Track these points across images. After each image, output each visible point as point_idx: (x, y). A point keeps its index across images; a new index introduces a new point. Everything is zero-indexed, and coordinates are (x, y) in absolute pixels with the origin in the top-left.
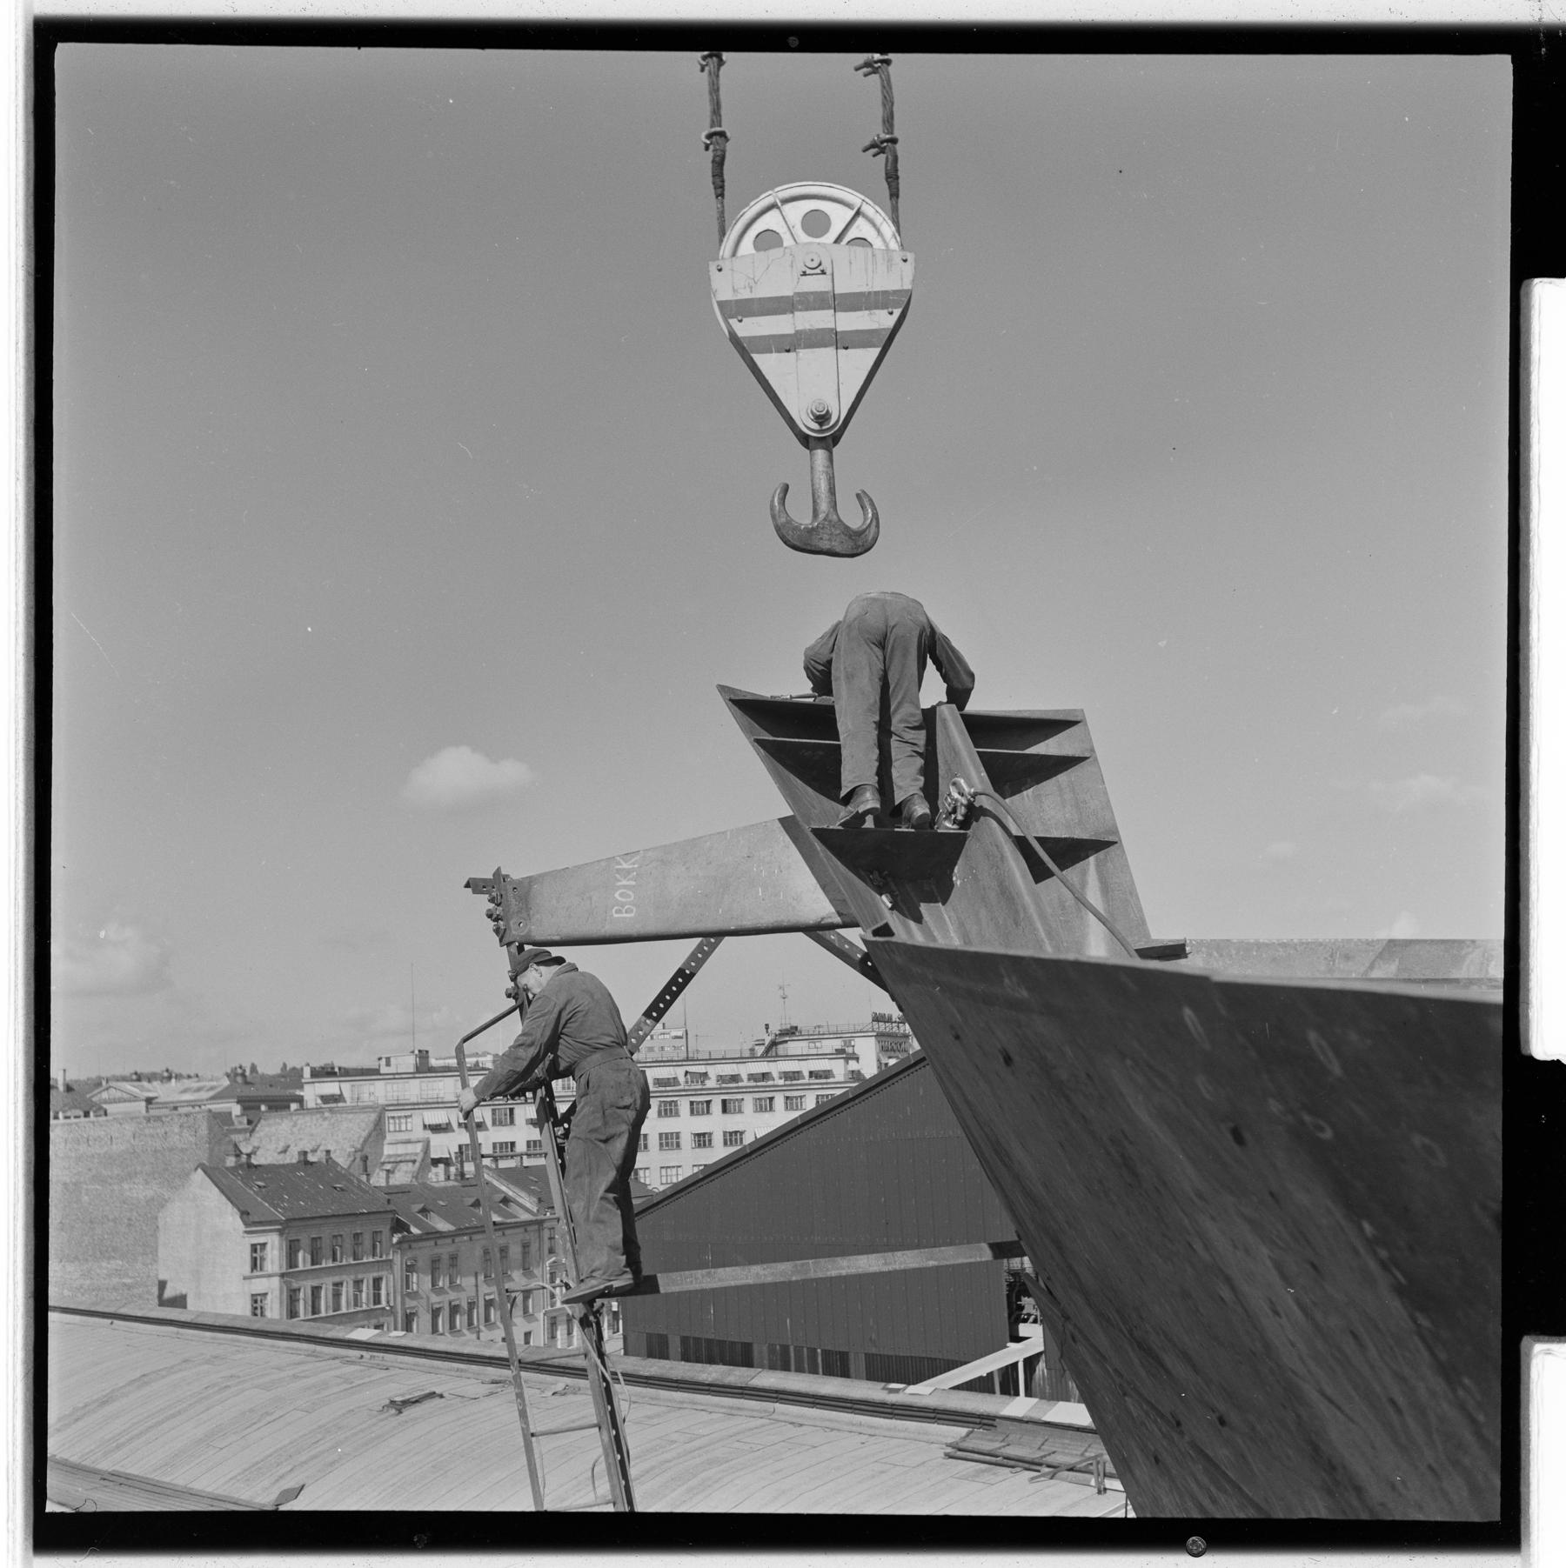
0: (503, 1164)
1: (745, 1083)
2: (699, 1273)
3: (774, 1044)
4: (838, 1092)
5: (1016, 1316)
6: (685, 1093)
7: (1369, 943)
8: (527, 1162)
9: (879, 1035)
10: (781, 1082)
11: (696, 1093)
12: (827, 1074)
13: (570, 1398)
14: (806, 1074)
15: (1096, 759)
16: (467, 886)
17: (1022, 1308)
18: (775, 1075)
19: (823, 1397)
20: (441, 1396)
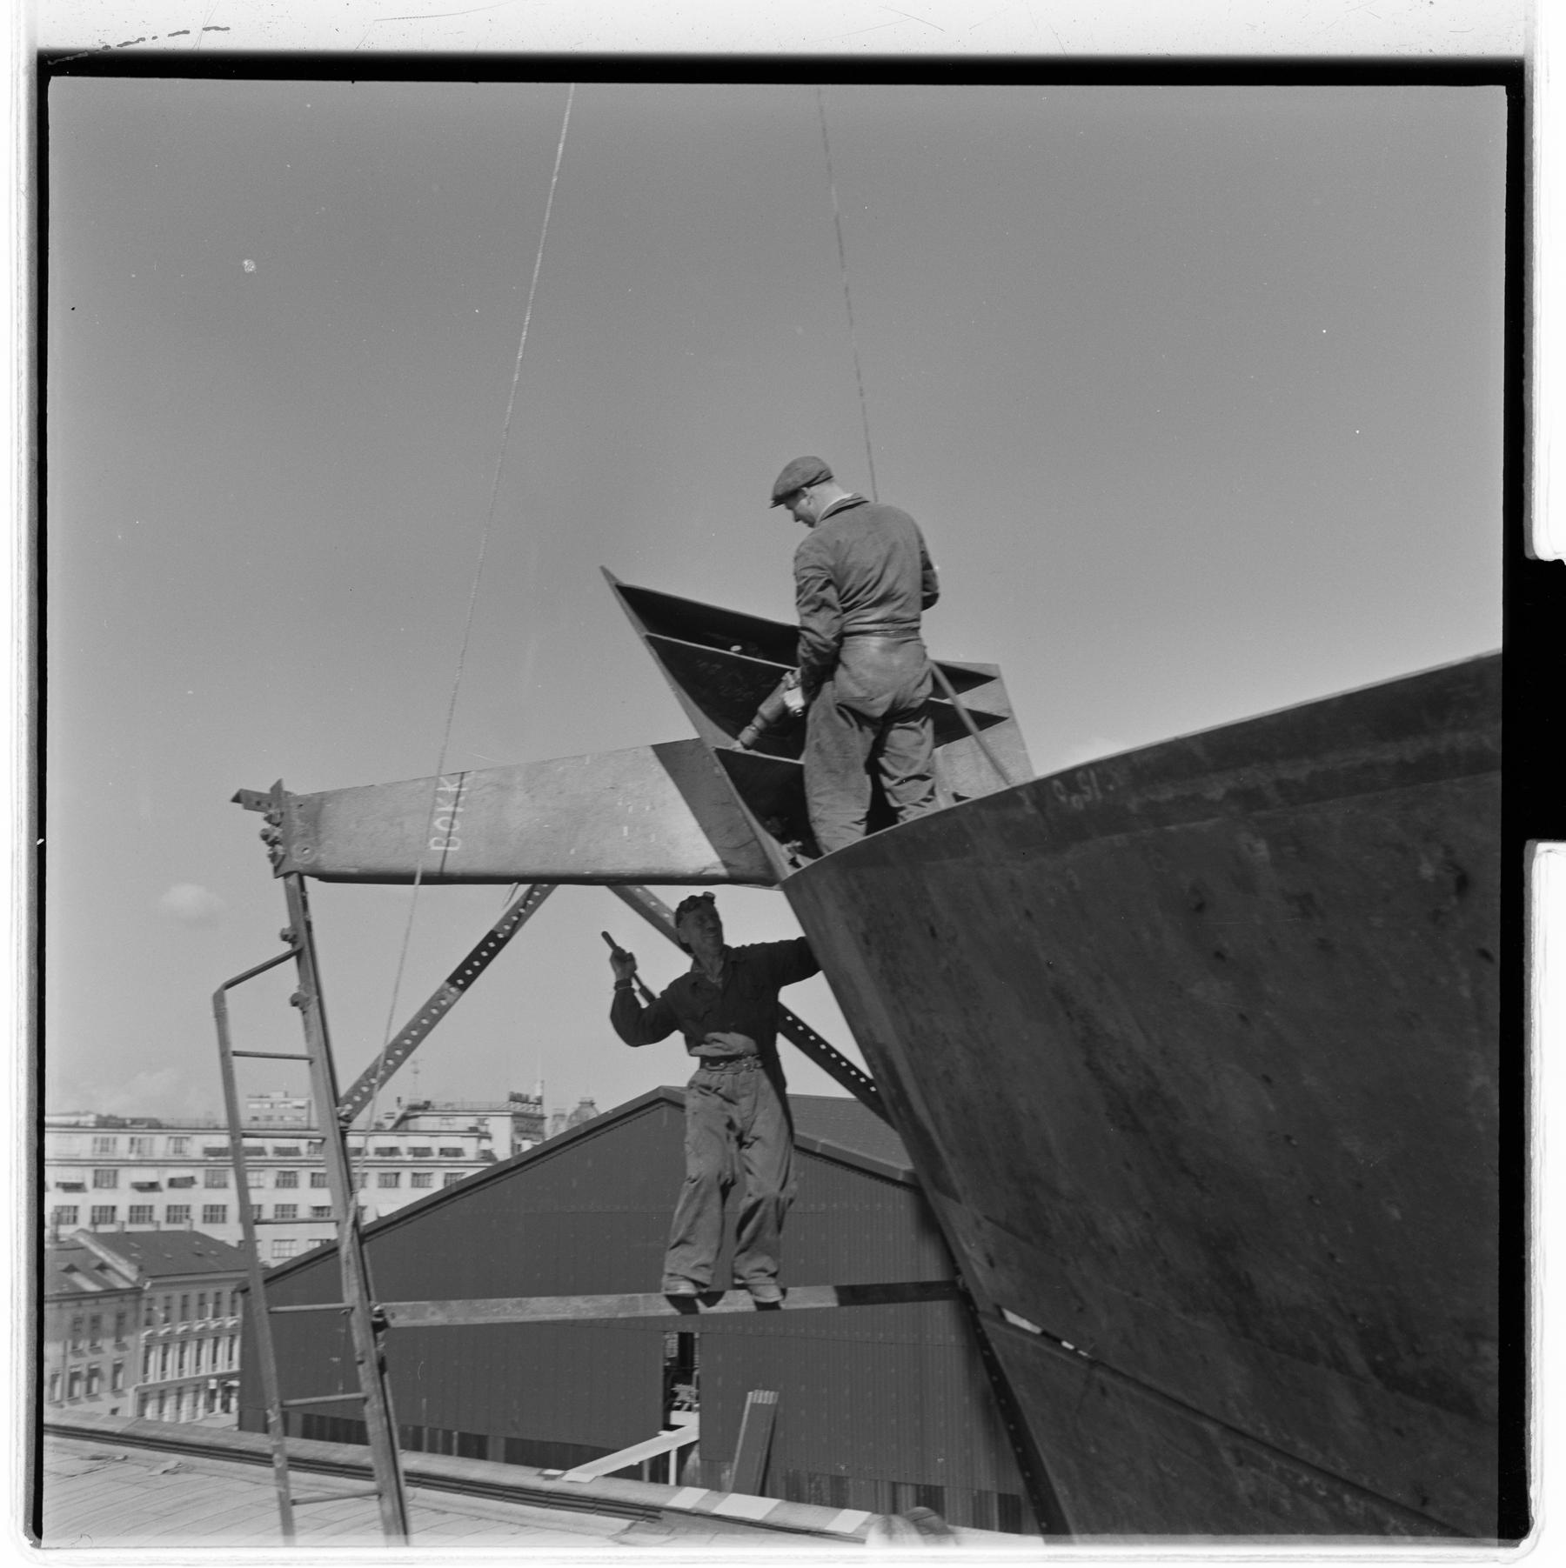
0: (102, 1229)
1: (372, 1157)
3: (405, 1118)
4: (470, 1172)
5: (670, 1402)
8: (129, 1228)
10: (410, 1158)
12: (457, 1152)
13: (182, 1477)
14: (436, 1151)
15: (1014, 722)
16: (237, 799)
17: (675, 1395)
18: (403, 1150)
19: (471, 1483)
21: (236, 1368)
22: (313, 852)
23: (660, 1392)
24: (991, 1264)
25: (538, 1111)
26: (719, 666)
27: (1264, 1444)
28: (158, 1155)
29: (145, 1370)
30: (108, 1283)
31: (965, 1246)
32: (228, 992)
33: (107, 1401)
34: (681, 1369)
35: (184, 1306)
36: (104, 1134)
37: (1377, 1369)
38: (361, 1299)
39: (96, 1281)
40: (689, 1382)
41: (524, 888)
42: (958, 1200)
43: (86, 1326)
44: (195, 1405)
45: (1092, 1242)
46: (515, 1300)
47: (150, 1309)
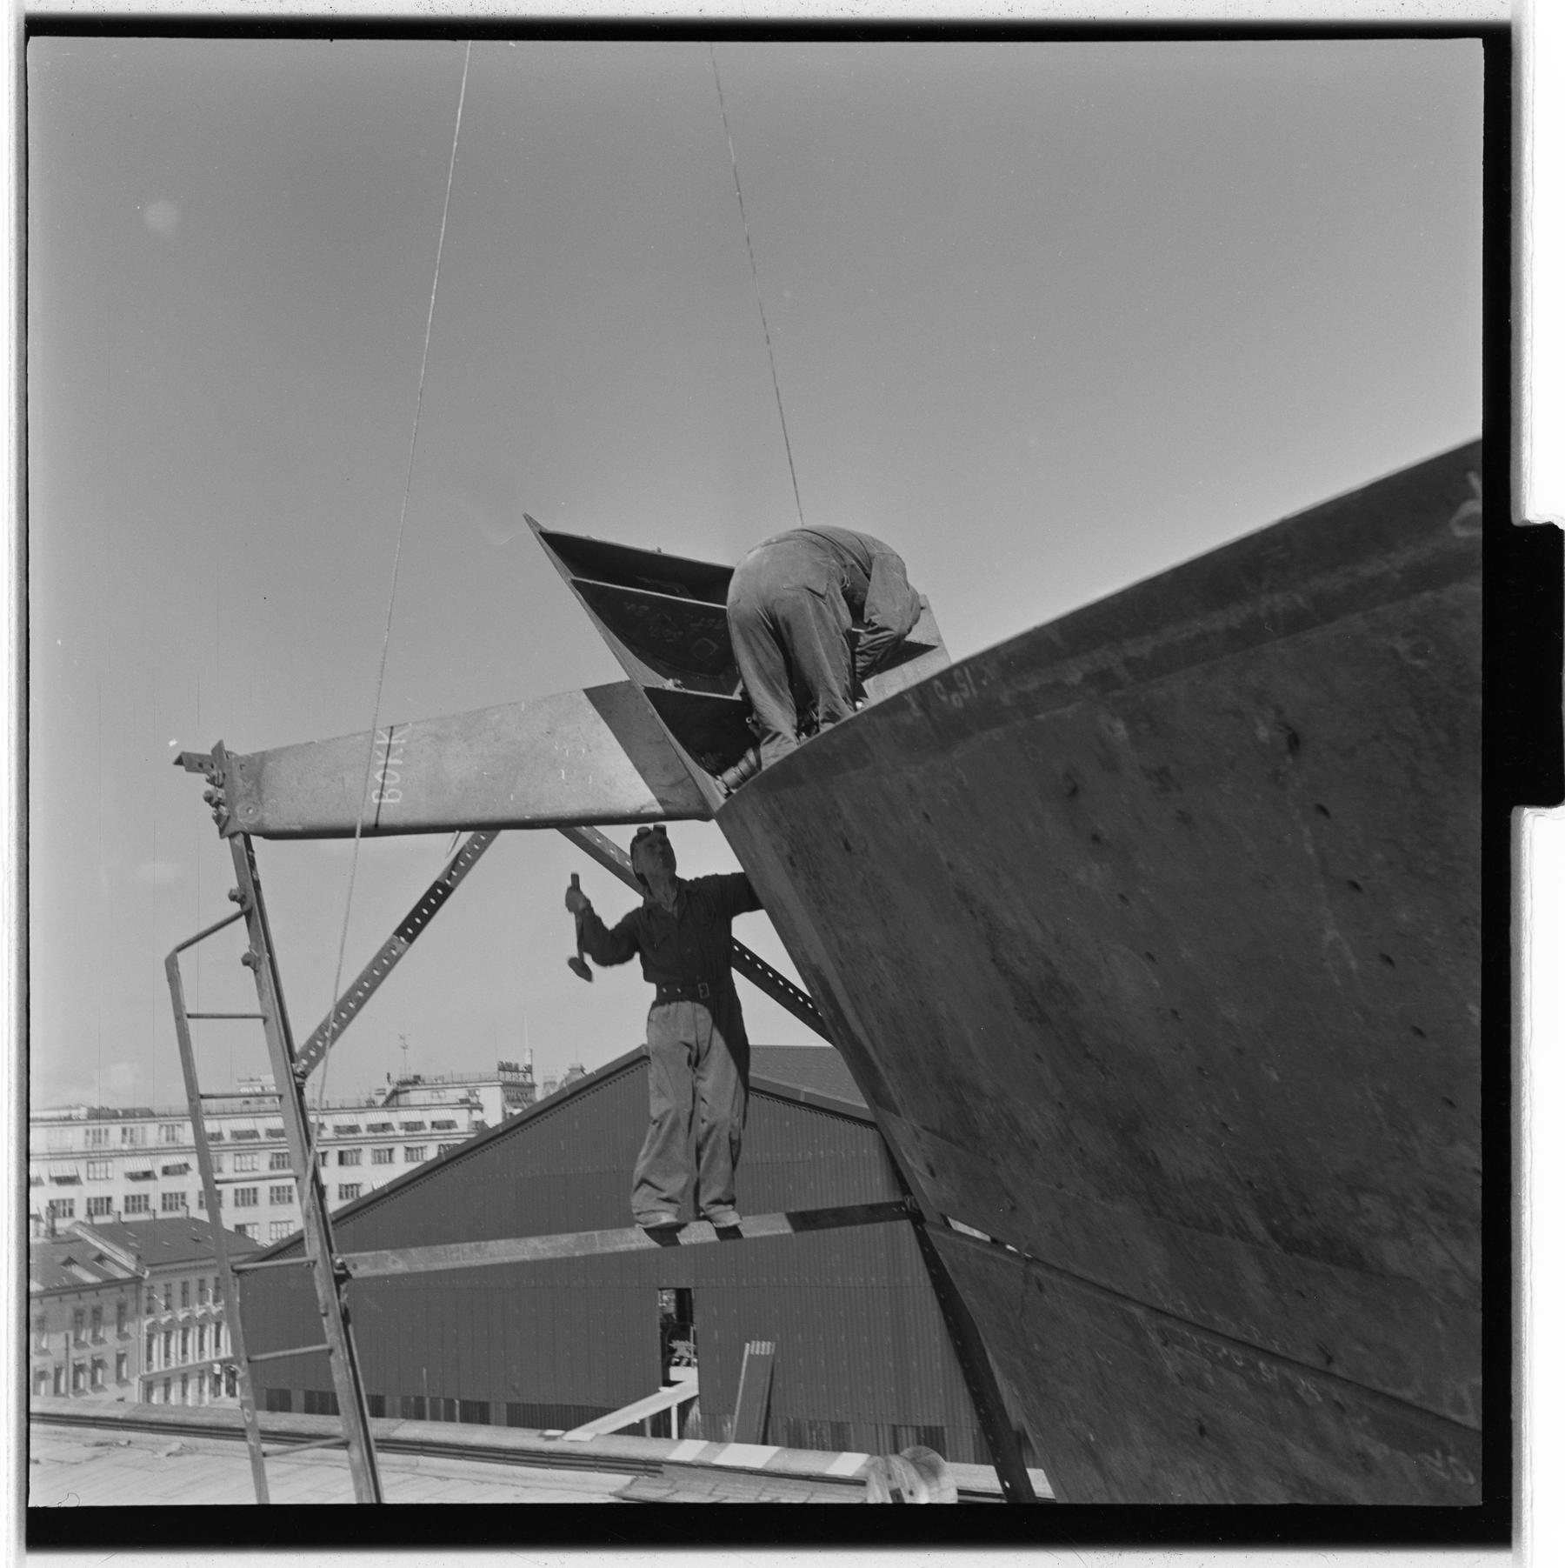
0: (98, 1220)
1: (364, 1133)
2: (467, 1246)
3: (395, 1093)
5: (668, 1358)
8: (124, 1218)
9: (506, 1086)
10: (402, 1133)
12: (450, 1124)
13: (187, 1458)
14: (428, 1124)
16: (179, 762)
17: (673, 1351)
18: (396, 1125)
19: (473, 1448)
23: (659, 1348)
24: (932, 1173)
25: (529, 1080)
26: (646, 608)
27: (1183, 1321)
28: (151, 1144)
29: (149, 1358)
30: (107, 1273)
31: (908, 1159)
32: (180, 955)
33: (113, 1391)
34: (678, 1325)
35: (185, 1292)
36: (95, 1126)
37: (1275, 1234)
38: (323, 1253)
40: (685, 1338)
41: (466, 836)
42: (898, 1114)
43: (88, 1316)
44: (201, 1390)
45: (1017, 1139)
47: (150, 1298)
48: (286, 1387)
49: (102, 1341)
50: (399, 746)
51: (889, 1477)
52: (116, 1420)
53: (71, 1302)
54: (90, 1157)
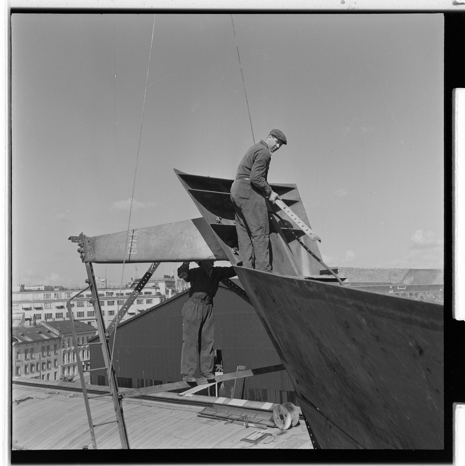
0: (49, 320)
1: (125, 296)
6: (106, 298)
7: (403, 270)
8: (56, 320)
11: (110, 298)
12: (150, 293)
13: (75, 398)
15: (301, 202)
16: (70, 239)
17: (217, 367)
20: (32, 398)
21: (89, 359)
22: (93, 255)
24: (298, 382)
29: (64, 360)
39: (47, 336)
40: (220, 364)
43: (46, 348)
46: (159, 386)
47: (64, 343)
48: (104, 375)
49: (50, 355)
50: (136, 236)
51: (279, 411)
52: (54, 386)
53: (41, 344)
54: (45, 302)
